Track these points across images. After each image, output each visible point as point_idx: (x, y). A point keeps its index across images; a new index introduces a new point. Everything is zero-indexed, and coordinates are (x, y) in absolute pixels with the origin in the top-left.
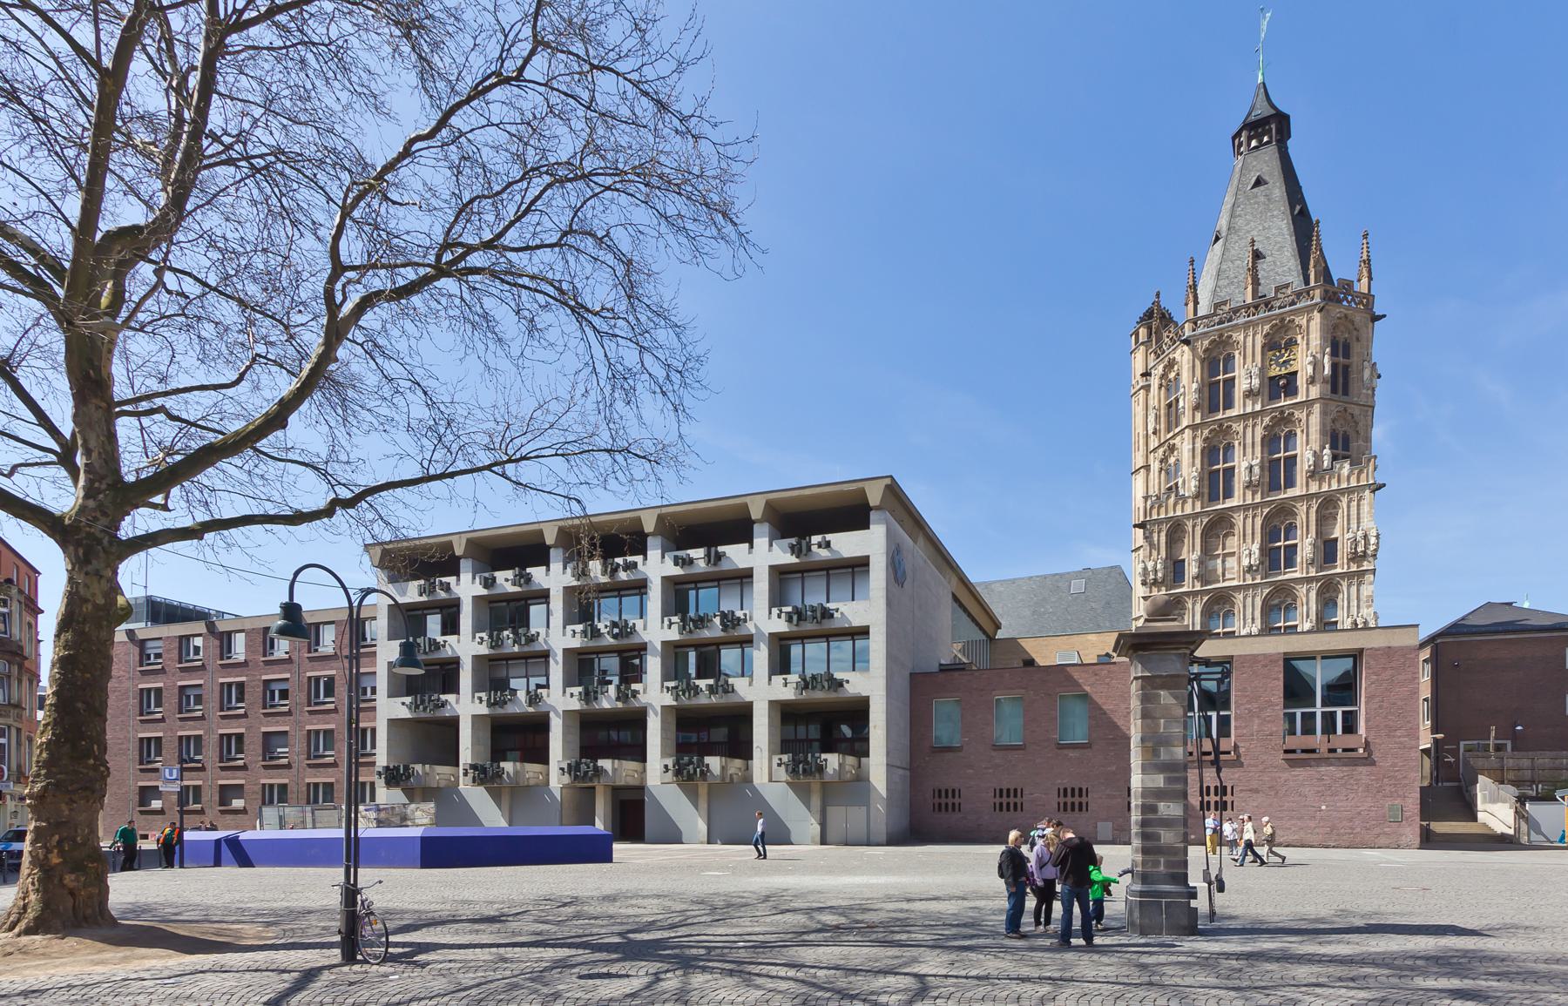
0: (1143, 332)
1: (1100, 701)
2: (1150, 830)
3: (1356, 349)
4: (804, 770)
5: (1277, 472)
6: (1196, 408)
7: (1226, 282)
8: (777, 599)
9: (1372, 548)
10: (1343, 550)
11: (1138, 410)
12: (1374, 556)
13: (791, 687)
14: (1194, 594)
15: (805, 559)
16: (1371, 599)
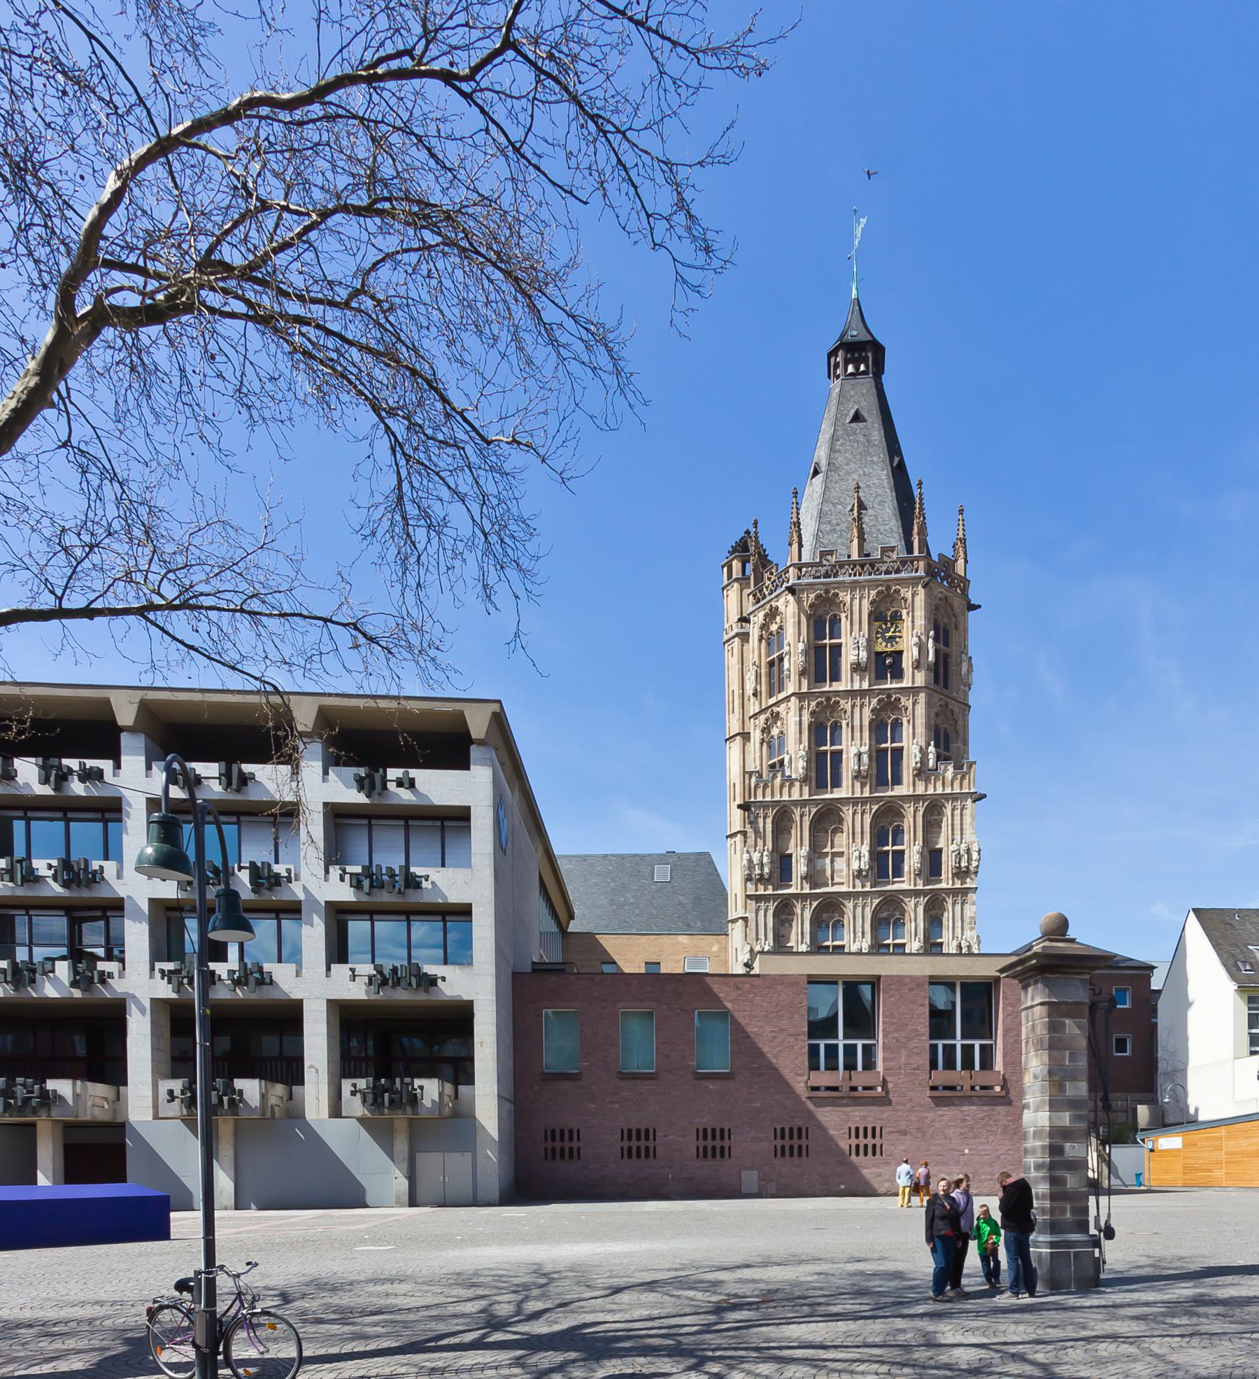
0: (736, 565)
1: (743, 1022)
2: (1058, 1173)
3: (954, 638)
4: (392, 1101)
5: (884, 766)
6: (802, 674)
7: (828, 528)
8: (334, 855)
9: (974, 864)
10: (948, 864)
11: (732, 662)
12: (976, 873)
13: (361, 983)
14: (802, 897)
15: (377, 800)
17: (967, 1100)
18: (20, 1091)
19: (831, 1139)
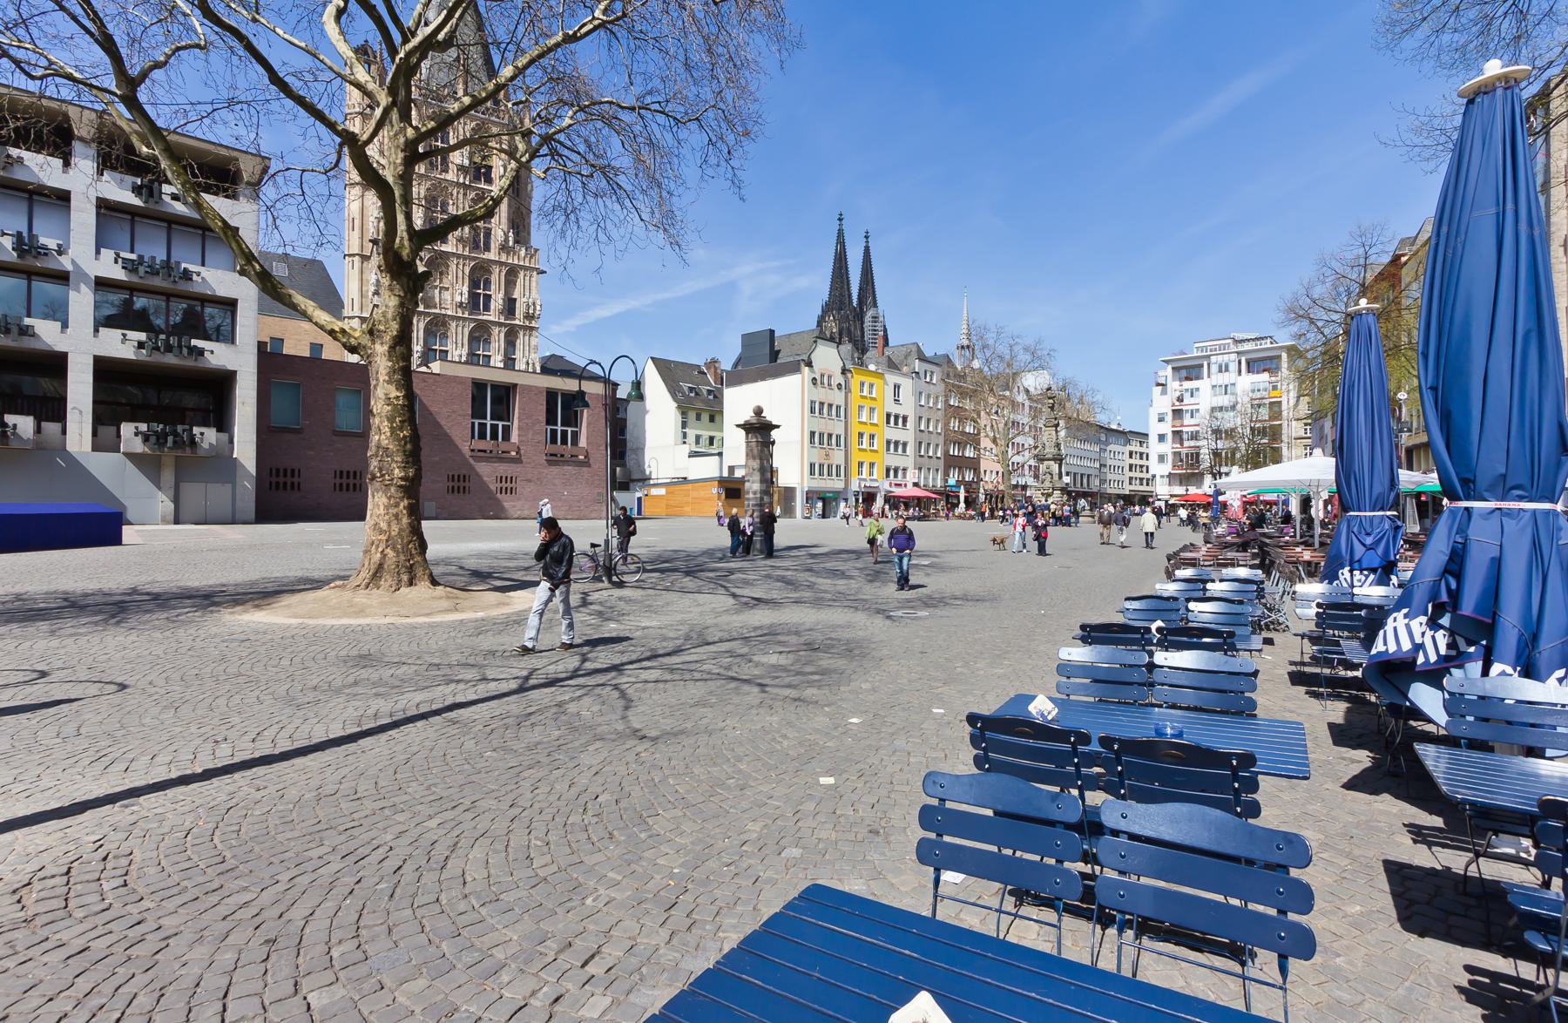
10: (520, 310)
15: (151, 206)
16: (536, 348)
17: (566, 463)
18: (1097, 482)
19: (484, 483)
